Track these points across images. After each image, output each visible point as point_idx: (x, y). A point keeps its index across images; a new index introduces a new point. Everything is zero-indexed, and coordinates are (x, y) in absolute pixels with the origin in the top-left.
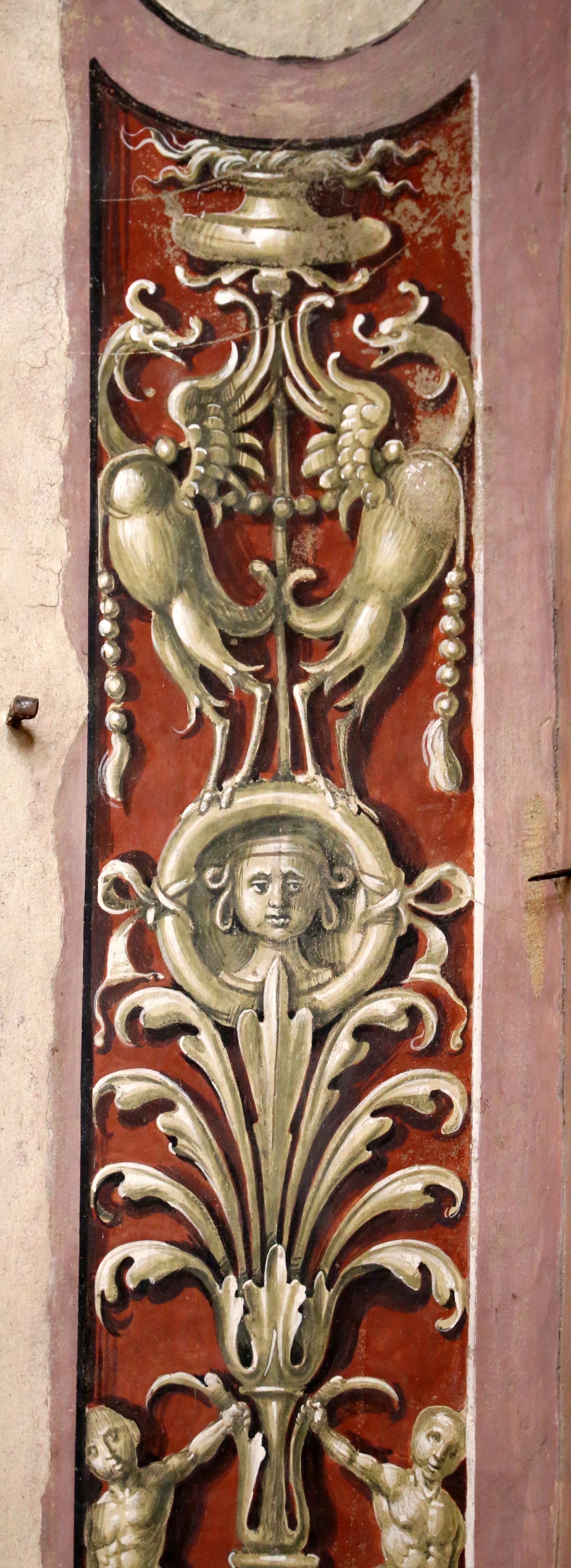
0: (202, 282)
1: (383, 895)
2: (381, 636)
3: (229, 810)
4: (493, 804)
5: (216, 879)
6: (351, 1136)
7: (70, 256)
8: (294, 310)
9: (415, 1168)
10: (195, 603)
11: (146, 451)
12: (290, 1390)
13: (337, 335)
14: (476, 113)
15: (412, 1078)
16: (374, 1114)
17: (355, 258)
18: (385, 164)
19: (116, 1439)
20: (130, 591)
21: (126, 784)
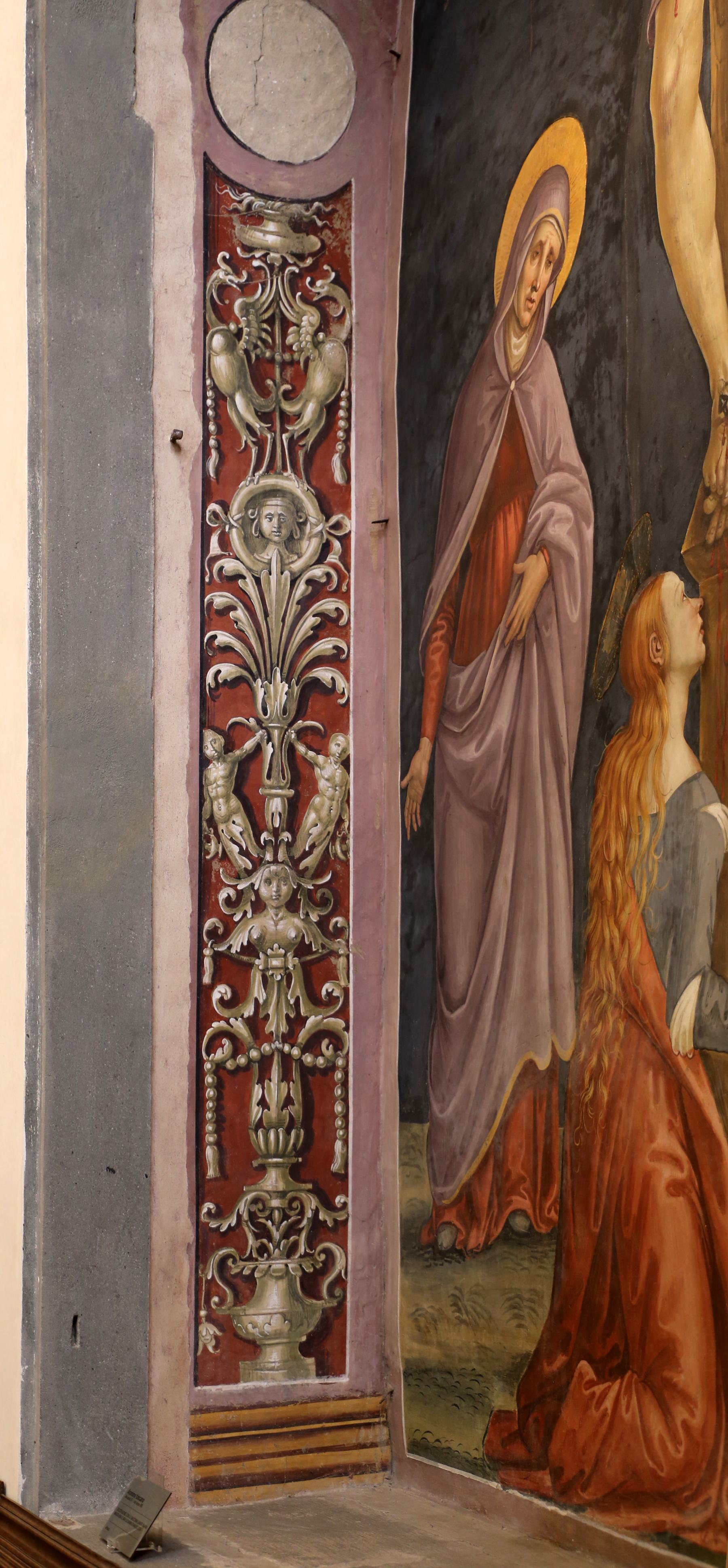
0: (247, 256)
1: (317, 525)
2: (316, 416)
3: (258, 486)
4: (358, 492)
5: (253, 514)
6: (305, 624)
7: (195, 239)
8: (283, 273)
9: (329, 639)
10: (244, 395)
11: (225, 327)
12: (282, 726)
13: (300, 285)
14: (353, 195)
15: (328, 602)
16: (314, 616)
17: (307, 253)
18: (318, 212)
19: (215, 743)
20: (219, 388)
21: (217, 471)
